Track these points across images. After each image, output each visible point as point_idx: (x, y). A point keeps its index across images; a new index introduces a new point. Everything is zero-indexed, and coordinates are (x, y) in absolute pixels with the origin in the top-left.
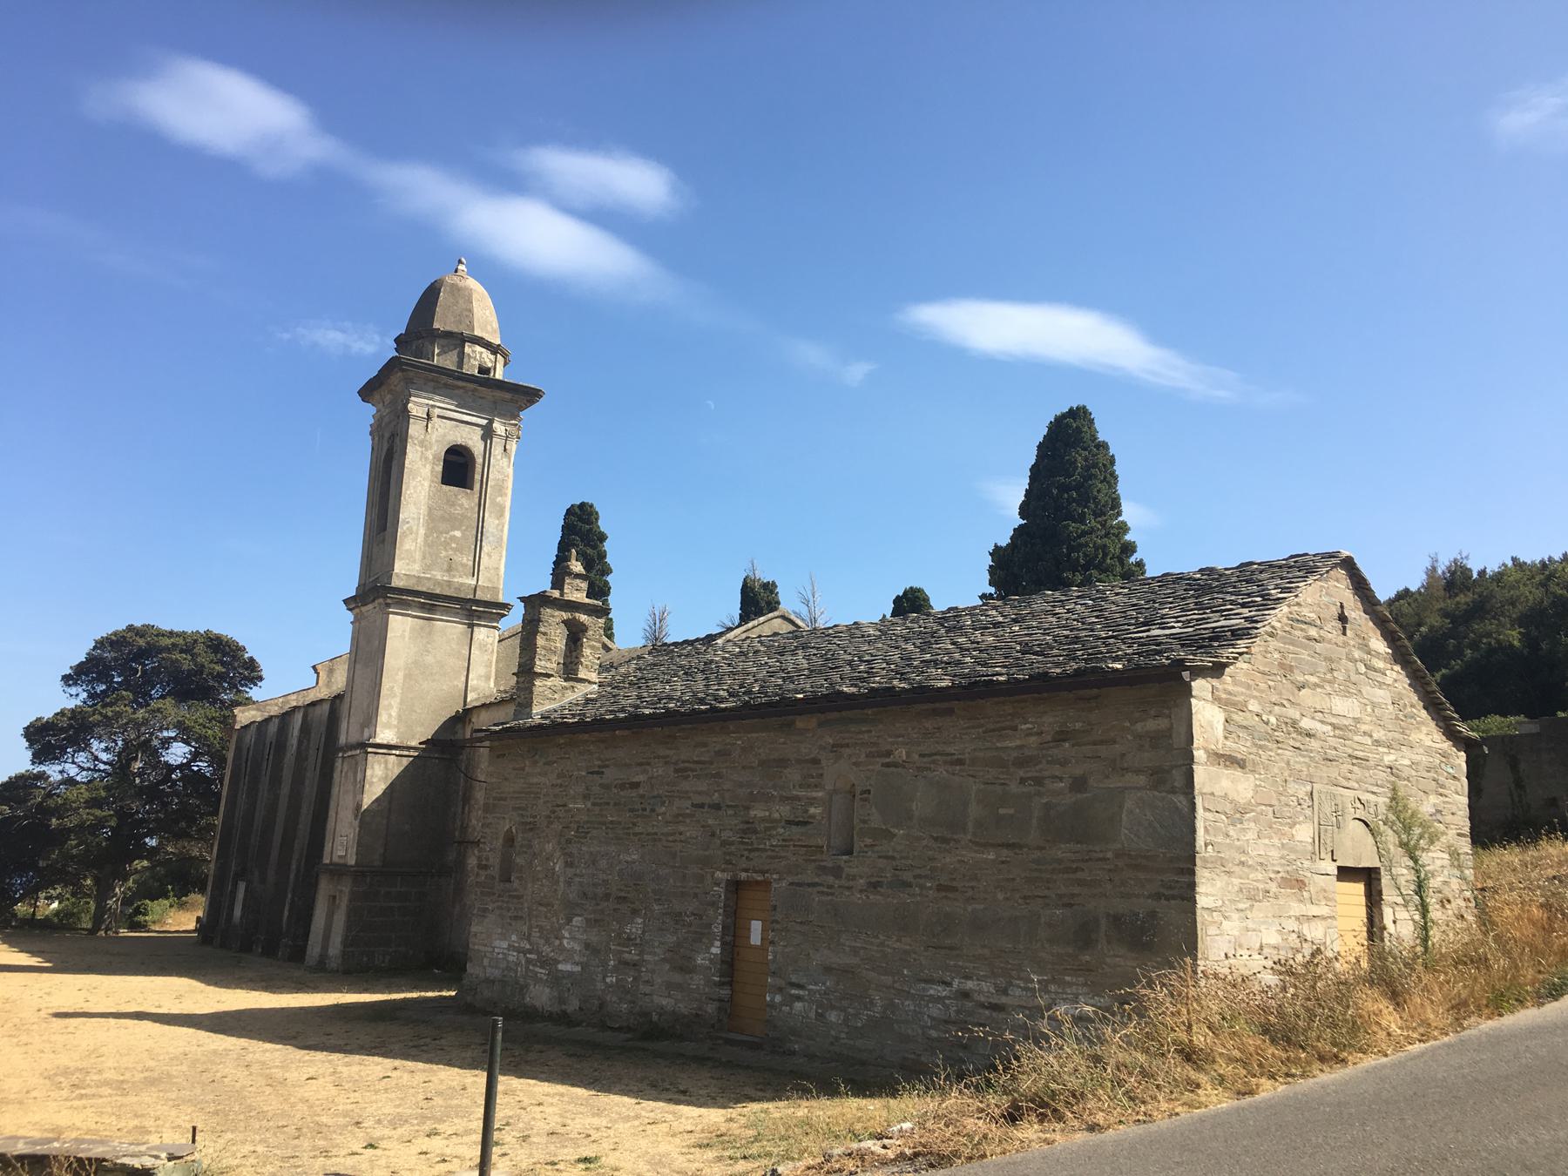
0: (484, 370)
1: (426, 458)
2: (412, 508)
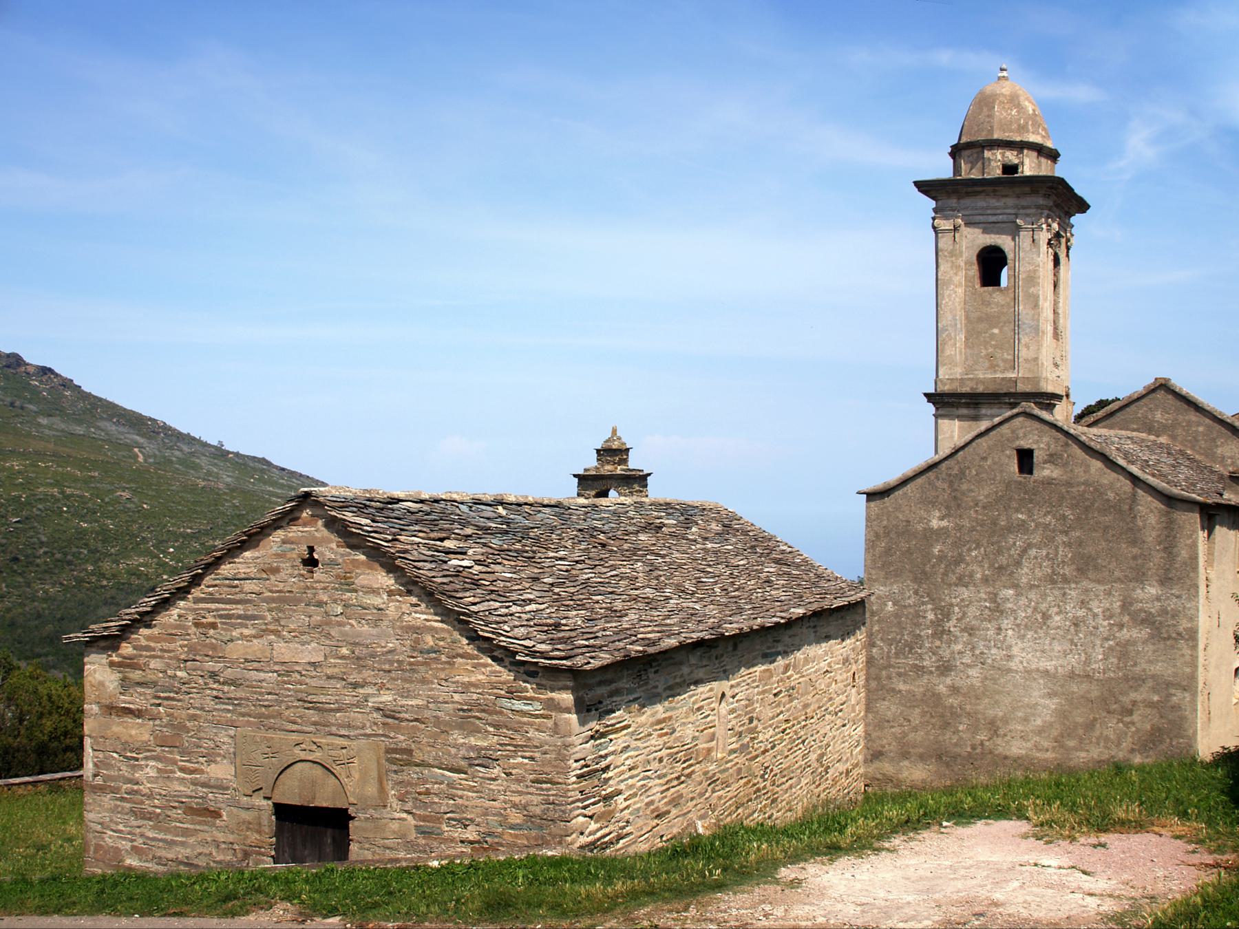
0: (1010, 169)
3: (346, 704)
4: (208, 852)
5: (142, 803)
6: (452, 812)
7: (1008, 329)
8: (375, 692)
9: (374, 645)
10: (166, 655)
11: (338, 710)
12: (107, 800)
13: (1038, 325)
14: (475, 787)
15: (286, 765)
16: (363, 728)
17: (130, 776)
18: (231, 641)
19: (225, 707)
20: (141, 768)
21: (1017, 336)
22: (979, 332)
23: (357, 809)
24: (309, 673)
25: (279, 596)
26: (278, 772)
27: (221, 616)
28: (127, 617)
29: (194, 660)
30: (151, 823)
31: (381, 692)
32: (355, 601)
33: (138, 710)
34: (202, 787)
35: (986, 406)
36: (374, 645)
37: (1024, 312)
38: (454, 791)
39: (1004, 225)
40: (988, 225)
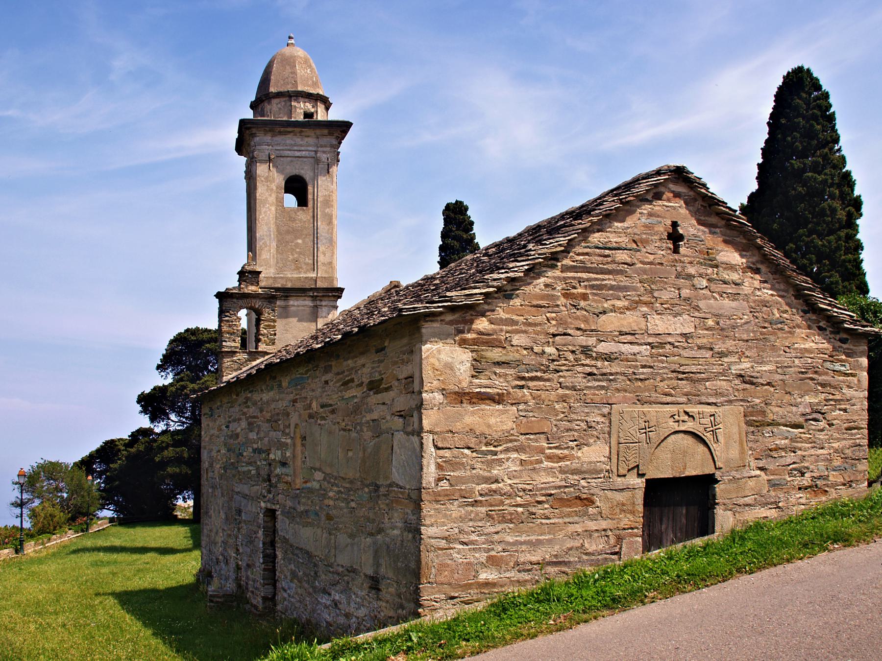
0: (308, 115)
1: (272, 190)
2: (265, 228)
3: (714, 373)
4: (579, 545)
5: (502, 503)
6: (794, 463)
7: (309, 240)
8: (737, 360)
9: (735, 317)
10: (530, 329)
11: (708, 380)
12: (455, 510)
13: (332, 238)
14: (810, 438)
15: (662, 438)
17: (486, 474)
18: (604, 312)
19: (597, 383)
20: (500, 462)
21: (315, 246)
22: (287, 242)
23: (722, 473)
24: (681, 344)
25: (651, 268)
27: (592, 287)
28: (495, 283)
29: (565, 334)
30: (511, 526)
31: (742, 360)
32: (715, 275)
33: (498, 394)
34: (572, 474)
35: (293, 298)
36: (735, 317)
37: (322, 227)
38: (796, 444)
39: (305, 160)
40: (294, 159)
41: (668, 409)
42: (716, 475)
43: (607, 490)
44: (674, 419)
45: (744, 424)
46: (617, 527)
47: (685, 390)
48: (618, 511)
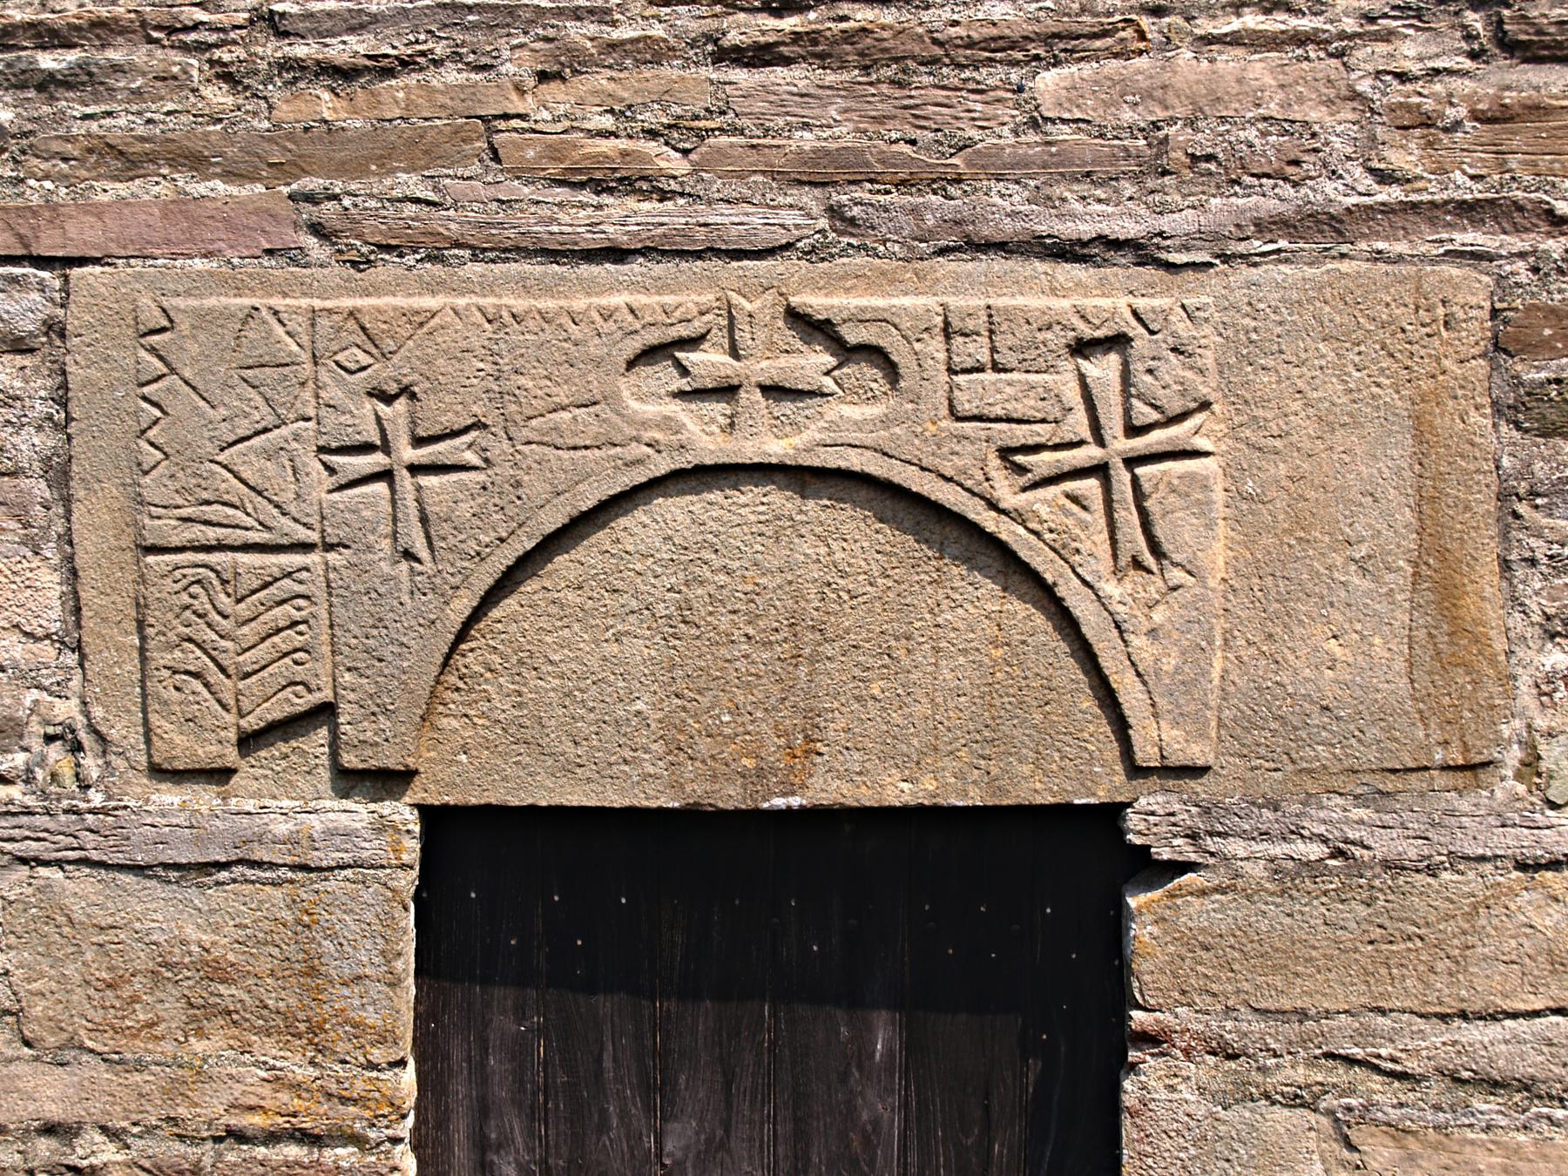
15: (553, 520)
16: (1287, 170)
26: (485, 578)
41: (618, 300)
42: (1133, 820)
43: (59, 863)
44: (684, 371)
45: (1481, 420)
46: (172, 1120)
47: (807, 140)
48: (172, 1009)
